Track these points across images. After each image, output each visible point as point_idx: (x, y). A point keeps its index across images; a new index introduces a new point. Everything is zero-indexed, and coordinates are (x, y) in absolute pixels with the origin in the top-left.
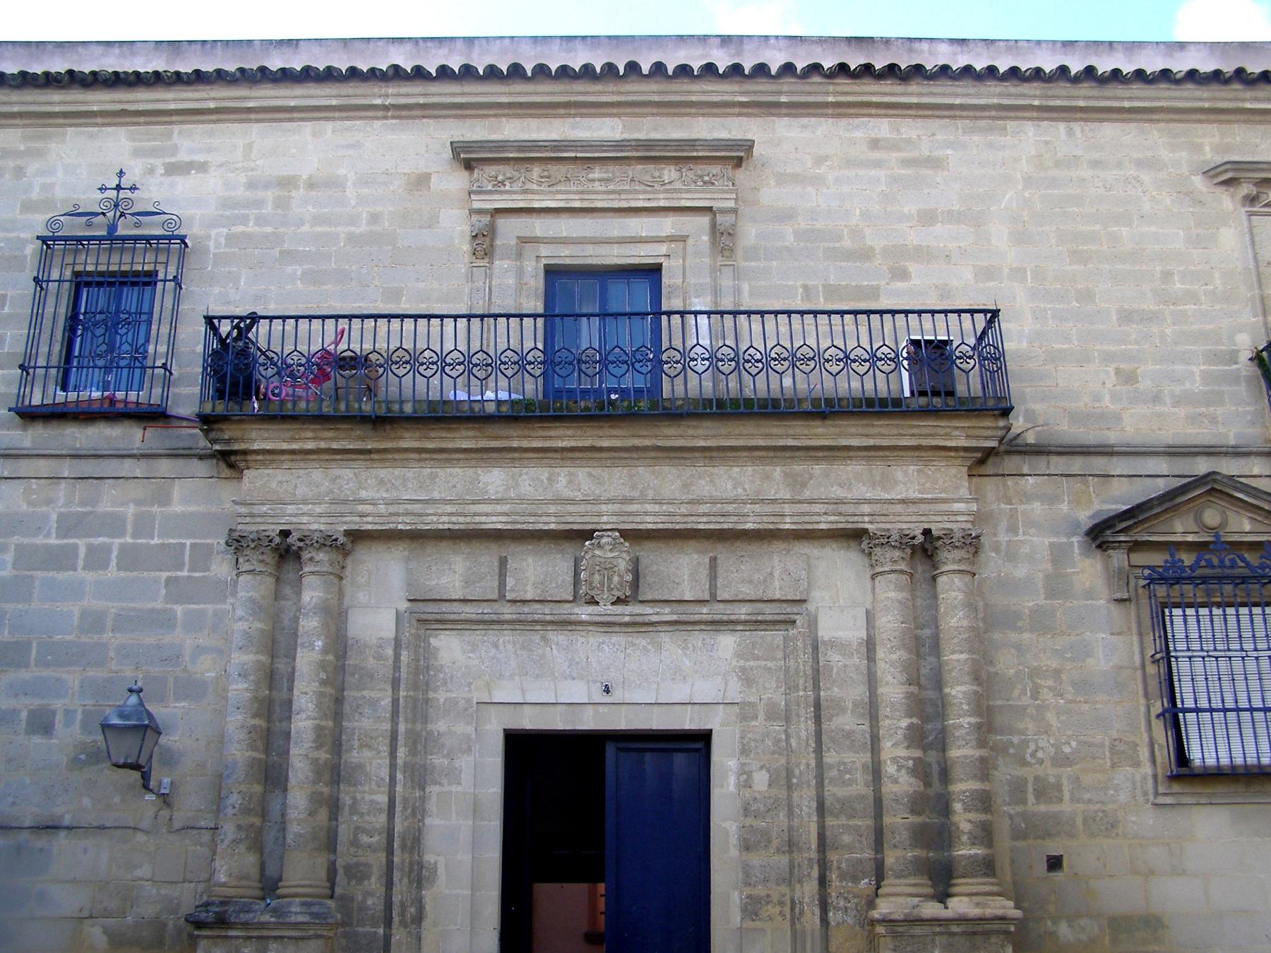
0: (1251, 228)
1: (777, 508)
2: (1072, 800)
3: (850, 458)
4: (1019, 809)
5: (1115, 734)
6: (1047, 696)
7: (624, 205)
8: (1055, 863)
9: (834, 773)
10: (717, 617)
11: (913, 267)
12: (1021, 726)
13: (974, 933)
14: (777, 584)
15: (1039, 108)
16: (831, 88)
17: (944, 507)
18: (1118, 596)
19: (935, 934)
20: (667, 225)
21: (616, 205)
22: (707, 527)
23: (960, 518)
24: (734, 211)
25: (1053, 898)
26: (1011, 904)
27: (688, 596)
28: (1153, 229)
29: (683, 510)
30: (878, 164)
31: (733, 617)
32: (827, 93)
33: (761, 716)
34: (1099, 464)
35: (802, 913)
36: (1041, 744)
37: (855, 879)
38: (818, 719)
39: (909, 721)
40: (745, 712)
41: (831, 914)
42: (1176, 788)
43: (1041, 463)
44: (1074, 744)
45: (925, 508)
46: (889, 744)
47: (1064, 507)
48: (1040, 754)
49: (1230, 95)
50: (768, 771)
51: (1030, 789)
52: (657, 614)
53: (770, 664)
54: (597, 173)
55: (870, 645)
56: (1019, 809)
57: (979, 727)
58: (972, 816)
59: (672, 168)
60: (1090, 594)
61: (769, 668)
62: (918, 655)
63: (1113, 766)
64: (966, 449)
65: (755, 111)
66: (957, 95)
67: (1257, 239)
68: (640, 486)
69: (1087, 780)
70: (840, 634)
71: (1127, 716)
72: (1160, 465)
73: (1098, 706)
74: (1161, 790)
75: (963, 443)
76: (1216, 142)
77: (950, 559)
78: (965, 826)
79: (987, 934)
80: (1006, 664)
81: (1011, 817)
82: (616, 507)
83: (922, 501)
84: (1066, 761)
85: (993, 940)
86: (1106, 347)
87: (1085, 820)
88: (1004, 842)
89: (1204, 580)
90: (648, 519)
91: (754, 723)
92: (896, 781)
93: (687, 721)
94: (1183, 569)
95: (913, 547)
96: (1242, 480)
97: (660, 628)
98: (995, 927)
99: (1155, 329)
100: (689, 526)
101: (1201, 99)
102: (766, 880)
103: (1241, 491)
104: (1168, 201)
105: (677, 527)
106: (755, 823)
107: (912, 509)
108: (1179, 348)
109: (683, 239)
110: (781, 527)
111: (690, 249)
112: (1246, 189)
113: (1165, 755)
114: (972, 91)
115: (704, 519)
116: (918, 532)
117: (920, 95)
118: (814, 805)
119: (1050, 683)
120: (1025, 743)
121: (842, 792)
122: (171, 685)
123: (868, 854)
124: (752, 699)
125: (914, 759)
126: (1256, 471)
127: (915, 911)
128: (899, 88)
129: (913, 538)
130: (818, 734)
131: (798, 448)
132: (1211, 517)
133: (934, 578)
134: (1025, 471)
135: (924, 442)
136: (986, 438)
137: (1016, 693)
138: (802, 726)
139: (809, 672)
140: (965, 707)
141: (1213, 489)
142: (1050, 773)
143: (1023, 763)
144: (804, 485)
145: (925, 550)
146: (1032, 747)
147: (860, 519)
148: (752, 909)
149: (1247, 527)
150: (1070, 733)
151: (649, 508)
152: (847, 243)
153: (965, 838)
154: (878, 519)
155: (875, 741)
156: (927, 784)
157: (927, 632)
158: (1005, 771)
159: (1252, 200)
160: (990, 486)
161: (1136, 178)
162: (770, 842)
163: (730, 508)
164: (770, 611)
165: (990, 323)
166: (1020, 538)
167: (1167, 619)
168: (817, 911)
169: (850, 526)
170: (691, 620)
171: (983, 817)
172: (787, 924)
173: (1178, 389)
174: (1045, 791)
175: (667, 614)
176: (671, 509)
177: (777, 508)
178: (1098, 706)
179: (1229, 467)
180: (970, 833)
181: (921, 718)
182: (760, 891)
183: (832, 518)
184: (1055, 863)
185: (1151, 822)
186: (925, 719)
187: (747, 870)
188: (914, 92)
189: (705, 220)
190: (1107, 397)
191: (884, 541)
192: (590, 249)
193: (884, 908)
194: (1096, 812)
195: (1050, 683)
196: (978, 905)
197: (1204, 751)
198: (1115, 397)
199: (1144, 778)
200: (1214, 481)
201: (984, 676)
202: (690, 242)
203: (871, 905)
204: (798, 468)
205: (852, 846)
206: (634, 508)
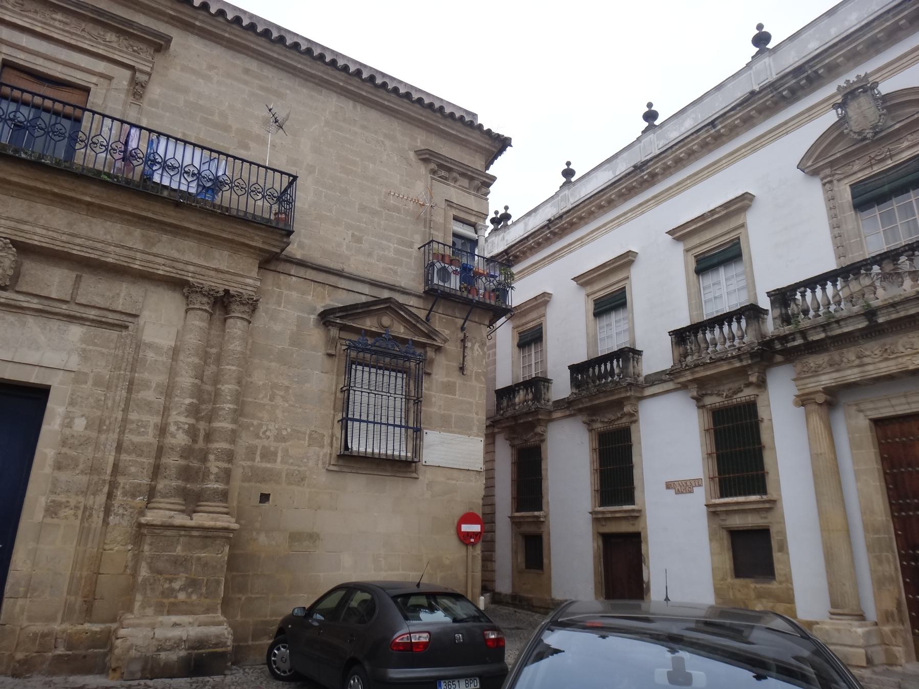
0: (431, 185)
1: (132, 254)
3: (188, 237)
4: (249, 463)
5: (313, 428)
6: (279, 401)
7: (73, 42)
8: (265, 498)
9: (134, 426)
10: (72, 313)
11: (252, 145)
12: (260, 415)
13: (206, 537)
14: (121, 301)
15: (342, 88)
16: (228, 29)
17: (239, 279)
18: (330, 352)
19: (180, 536)
20: (101, 67)
21: (67, 40)
22: (79, 253)
23: (248, 288)
24: (149, 74)
25: (260, 519)
26: (234, 520)
27: (53, 296)
29: (64, 238)
30: (246, 83)
31: (84, 315)
32: (225, 31)
33: (90, 382)
34: (333, 280)
35: (90, 516)
36: (270, 427)
37: (134, 496)
38: (130, 390)
39: (191, 400)
40: (79, 377)
41: (111, 518)
42: (341, 462)
43: (302, 272)
44: (289, 430)
45: (228, 276)
46: (175, 413)
47: (310, 298)
48: (268, 433)
50: (87, 418)
51: (258, 453)
52: (28, 302)
53: (104, 350)
54: (59, 16)
55: (175, 352)
56: (249, 463)
57: (235, 411)
58: (220, 464)
59: (114, 35)
61: (103, 353)
62: (205, 362)
63: (309, 445)
64: (261, 250)
65: (178, 24)
68: (35, 216)
69: (292, 452)
70: (157, 340)
71: (320, 416)
72: (366, 289)
74: (332, 462)
75: (260, 245)
76: (422, 140)
77: (237, 310)
78: (214, 470)
79: (215, 538)
80: (258, 378)
81: (244, 468)
82: (12, 224)
83: (228, 272)
84: (284, 439)
85: (218, 542)
87: (287, 475)
88: (236, 483)
89: (376, 352)
90: (36, 238)
91: (83, 386)
92: (174, 436)
93: (34, 377)
94: (367, 345)
95: (216, 298)
97: (28, 312)
98: (221, 534)
99: (376, 219)
100: (66, 250)
102: (68, 491)
105: (57, 248)
106: (69, 452)
107: (220, 275)
109: (110, 78)
110: (132, 266)
111: (113, 86)
112: (433, 166)
113: (338, 444)
114: (309, 64)
115: (78, 248)
116: (221, 290)
118: (115, 445)
119: (282, 393)
120: (260, 426)
121: (136, 439)
122: (284, 475)
123: (146, 481)
124: (86, 370)
125: (189, 424)
126: (411, 303)
127: (170, 520)
128: (268, 45)
129: (217, 292)
130: (128, 401)
131: (155, 221)
132: (386, 321)
133: (225, 320)
134: (292, 273)
135: (236, 238)
136: (274, 246)
137: (261, 396)
138: (118, 393)
139: (130, 359)
140: (229, 398)
141: (389, 307)
142: (272, 444)
143: (257, 436)
144: (154, 244)
145: (223, 302)
146: (264, 428)
147: (186, 274)
148: (52, 510)
149: (402, 330)
151: (38, 230)
152: (216, 118)
153: (212, 477)
154: (198, 276)
155: (166, 410)
156: (195, 441)
157: (214, 351)
158: (245, 440)
159: (434, 172)
160: (270, 276)
162: (77, 466)
163: (99, 245)
164: (111, 318)
165: (291, 184)
166: (281, 309)
167: (353, 371)
168: (102, 515)
169: (178, 276)
170: (49, 311)
171: (226, 465)
172: (78, 522)
173: (381, 253)
174: (268, 455)
175: (35, 304)
176: (55, 235)
177: (132, 254)
179: (400, 299)
180: (216, 474)
181: (199, 400)
182: (62, 498)
183: (168, 269)
184: (265, 498)
186: (201, 401)
187: (55, 483)
188: (276, 52)
189: (128, 73)
191: (201, 292)
192: (40, 61)
193: (151, 517)
195: (282, 393)
196: (212, 519)
197: (358, 445)
199: (325, 455)
201: (244, 383)
202: (115, 81)
203: (142, 513)
204: (152, 233)
205: (137, 472)
206: (26, 227)
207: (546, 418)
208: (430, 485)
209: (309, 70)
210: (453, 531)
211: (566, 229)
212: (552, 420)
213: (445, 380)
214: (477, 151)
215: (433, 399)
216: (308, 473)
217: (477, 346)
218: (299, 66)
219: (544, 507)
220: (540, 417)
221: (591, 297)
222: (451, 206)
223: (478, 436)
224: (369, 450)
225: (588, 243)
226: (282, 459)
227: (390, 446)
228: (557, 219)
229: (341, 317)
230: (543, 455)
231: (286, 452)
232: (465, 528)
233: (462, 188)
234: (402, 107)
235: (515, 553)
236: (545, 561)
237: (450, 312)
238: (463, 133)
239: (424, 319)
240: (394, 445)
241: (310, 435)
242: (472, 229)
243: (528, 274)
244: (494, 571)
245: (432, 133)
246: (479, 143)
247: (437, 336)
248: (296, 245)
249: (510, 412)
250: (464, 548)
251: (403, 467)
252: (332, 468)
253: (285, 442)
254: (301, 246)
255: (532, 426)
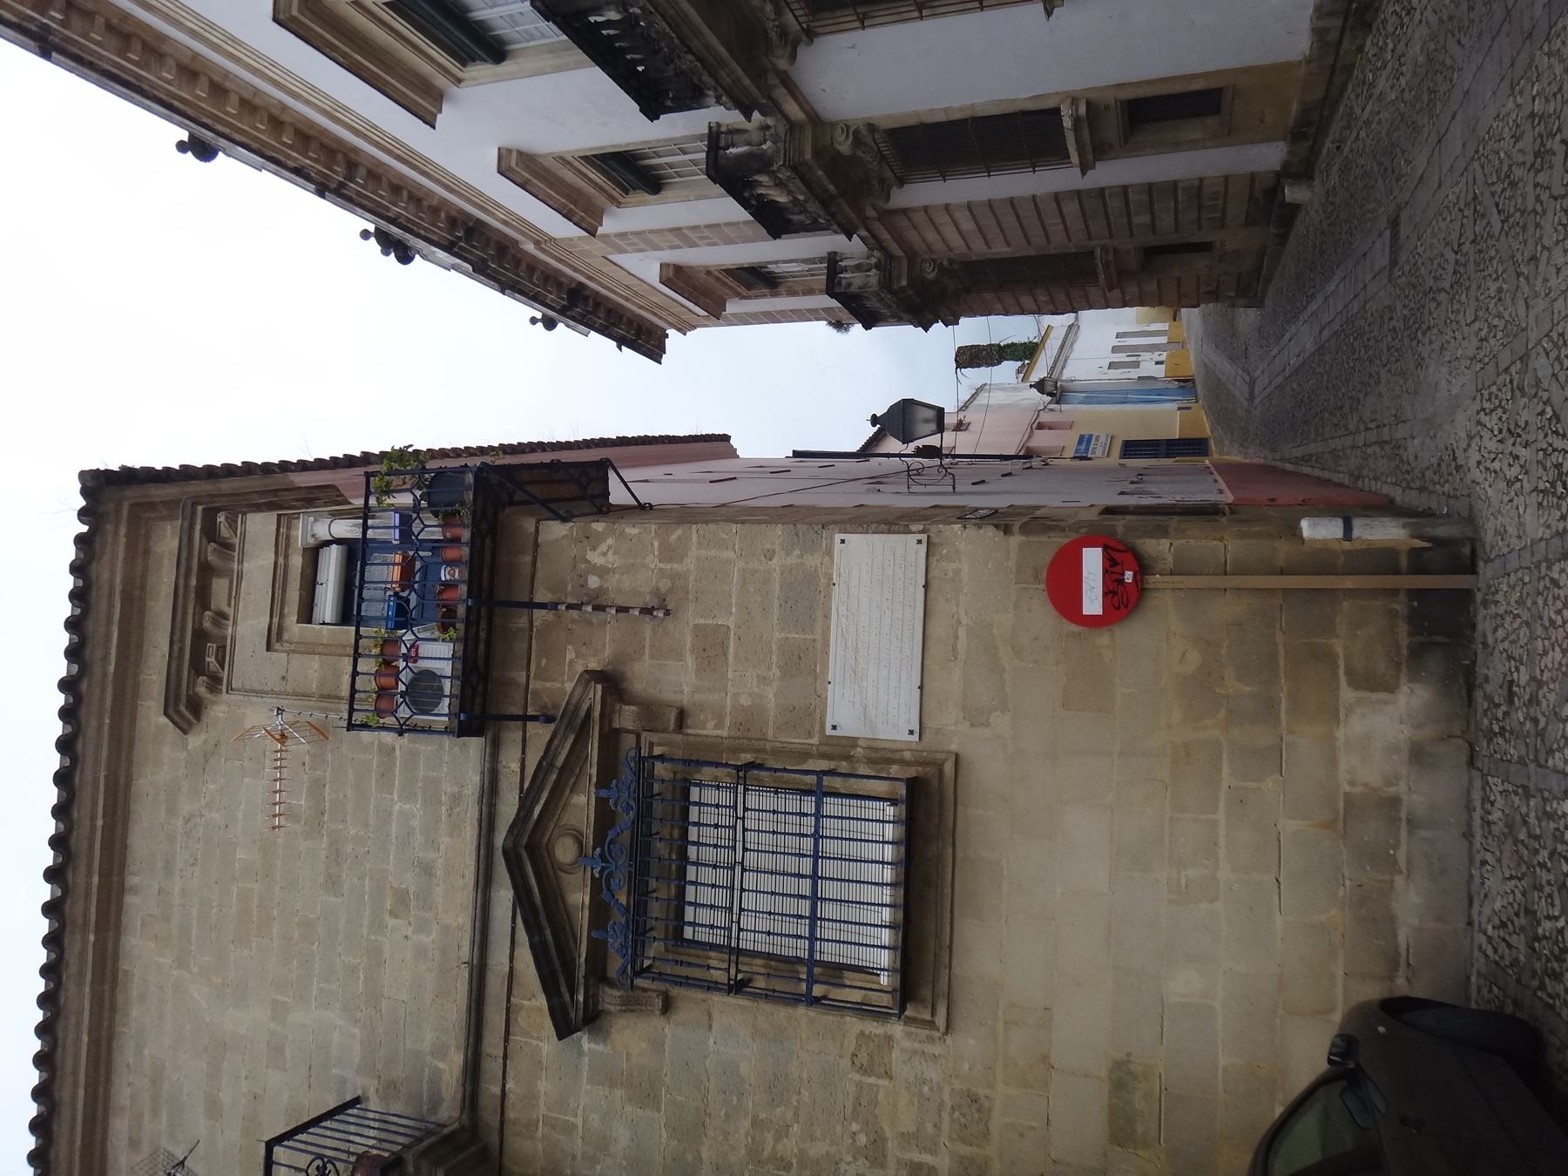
2: (933, 1152)
5: (845, 1062)
15: (101, 929)
28: (240, 816)
42: (926, 993)
43: (492, 1067)
44: (855, 1127)
49: (97, 691)
60: (657, 1045)
63: (888, 1075)
66: (78, 1038)
67: (257, 687)
69: (907, 1123)
71: (815, 1042)
73: (805, 1076)
74: (928, 1017)
76: (152, 715)
84: (878, 1141)
86: (366, 922)
87: (964, 1141)
96: (526, 785)
99: (349, 848)
101: (100, 728)
103: (532, 809)
104: (212, 787)
108: (372, 821)
114: (73, 1020)
117: (75, 1084)
119: (769, 1137)
122: (965, 1150)
126: (515, 766)
128: (65, 1114)
132: (565, 851)
134: (497, 1090)
150: (839, 1129)
159: (215, 682)
161: (187, 821)
173: (419, 838)
178: (805, 1076)
185: (972, 1041)
190: (422, 937)
194: (952, 1121)
198: (422, 927)
199: (909, 1035)
200: (516, 845)
207: (809, 133)
208: (976, 717)
209: (86, 1015)
210: (1103, 638)
211: (323, 146)
212: (815, 119)
213: (690, 661)
214: (147, 552)
215: (745, 701)
216: (957, 1085)
217: (595, 558)
218: (85, 1038)
219: (1051, 104)
220: (808, 156)
221: (460, 75)
222: (281, 628)
223: (829, 552)
224: (886, 915)
225: (326, 96)
226: (925, 1150)
227: (873, 851)
228: (308, 178)
229: (572, 991)
230: (913, 122)
231: (907, 1139)
232: (1093, 603)
233: (234, 596)
234: (96, 781)
235: (1176, 146)
236: (1197, 86)
237: (520, 647)
238: (111, 606)
239: (552, 726)
240: (871, 835)
241: (863, 1070)
242: (324, 552)
243: (481, 194)
244: (1226, 178)
245: (137, 686)
246: (121, 555)
247: (578, 707)
248: (441, 1065)
249: (813, 207)
250: (1154, 602)
251: (928, 805)
252: (941, 1021)
253: (884, 1139)
254: (440, 1051)
255: (835, 164)
